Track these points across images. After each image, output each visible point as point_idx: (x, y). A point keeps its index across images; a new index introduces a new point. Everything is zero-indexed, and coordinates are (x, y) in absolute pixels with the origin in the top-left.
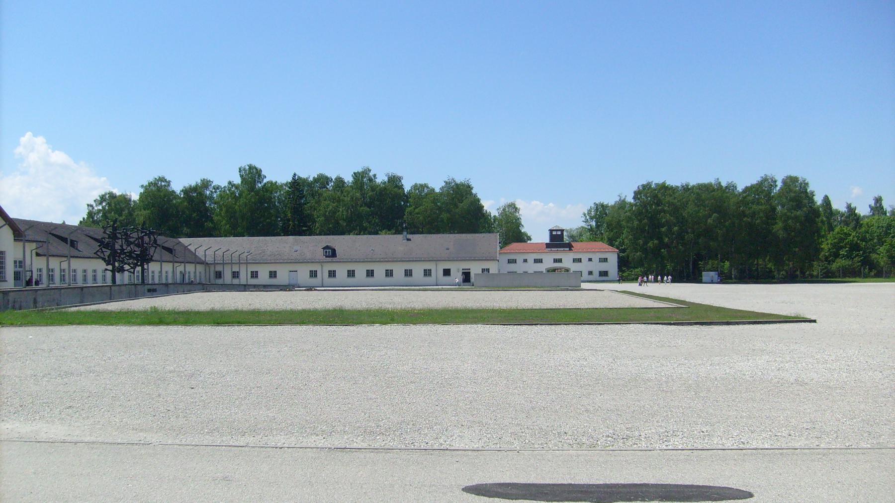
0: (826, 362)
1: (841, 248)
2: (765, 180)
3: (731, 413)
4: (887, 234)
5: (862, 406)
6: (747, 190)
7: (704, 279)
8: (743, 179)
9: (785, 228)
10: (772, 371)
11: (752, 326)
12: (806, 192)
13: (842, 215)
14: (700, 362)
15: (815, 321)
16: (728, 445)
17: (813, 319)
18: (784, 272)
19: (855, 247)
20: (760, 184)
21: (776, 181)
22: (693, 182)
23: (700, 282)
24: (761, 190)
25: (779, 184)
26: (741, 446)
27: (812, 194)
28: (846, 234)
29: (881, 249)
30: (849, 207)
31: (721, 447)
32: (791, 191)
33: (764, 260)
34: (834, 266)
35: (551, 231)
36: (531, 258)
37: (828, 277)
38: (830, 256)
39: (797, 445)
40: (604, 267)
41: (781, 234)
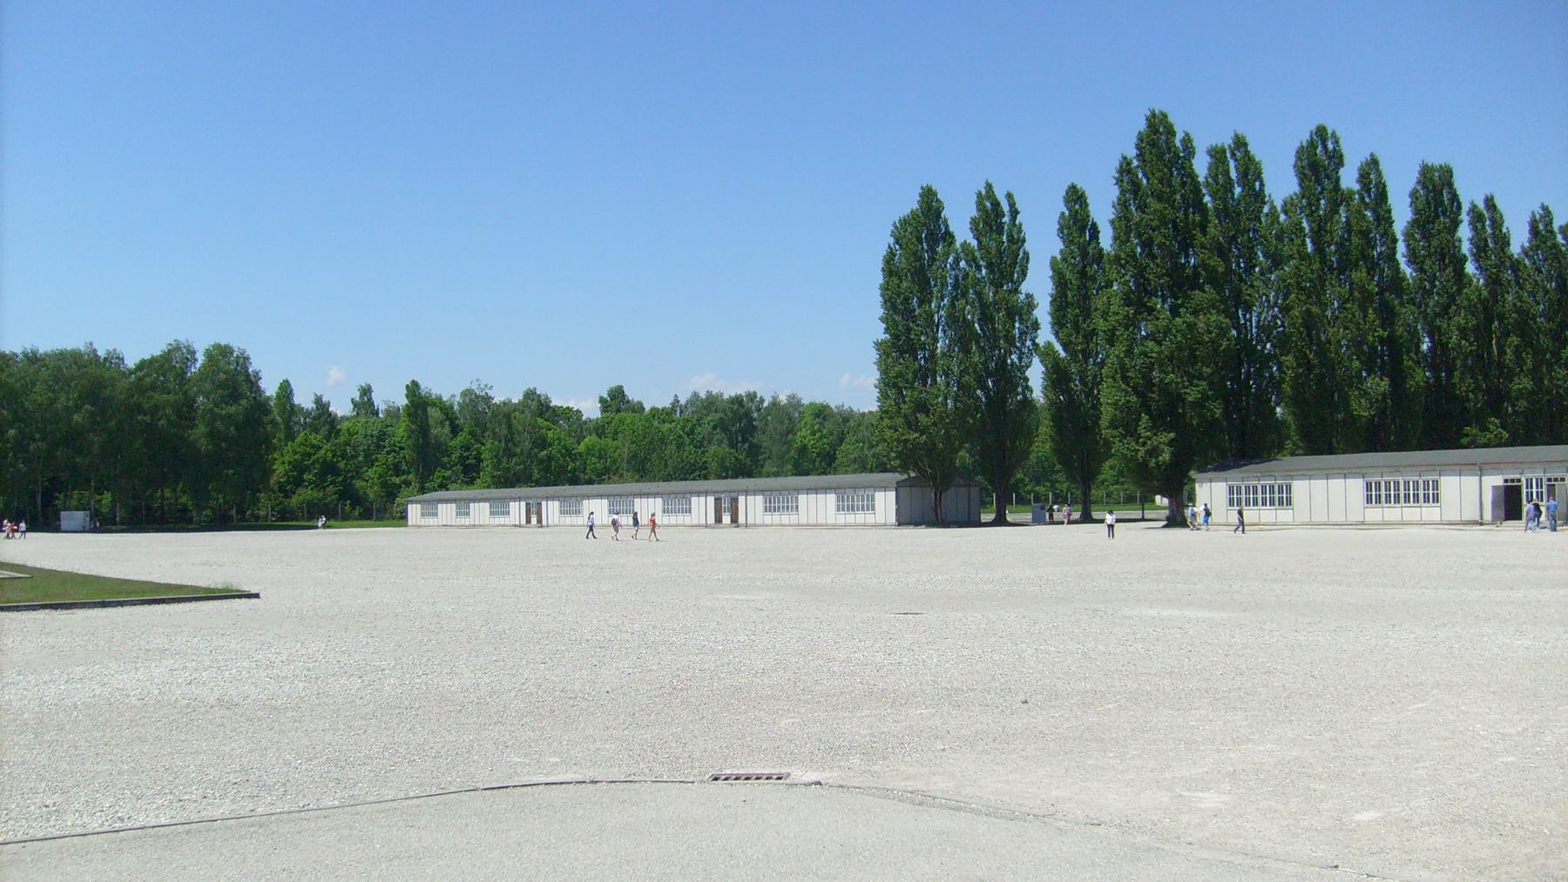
0: (271, 665)
1: (307, 469)
2: (175, 349)
3: (100, 768)
4: (379, 447)
5: (328, 737)
6: (142, 365)
7: (64, 524)
8: (133, 342)
9: (213, 435)
10: (179, 686)
11: (147, 608)
12: (248, 375)
13: (307, 414)
14: (47, 677)
15: (256, 596)
16: (94, 825)
17: (246, 588)
18: (208, 512)
19: (329, 468)
20: (167, 356)
21: (194, 353)
22: (46, 345)
23: (57, 530)
24: (167, 367)
25: (201, 358)
26: (118, 825)
27: (257, 377)
28: (313, 446)
29: (371, 473)
30: (318, 400)
31: (79, 830)
32: (219, 370)
33: (174, 490)
34: (295, 501)
37: (286, 519)
38: (288, 482)
39: (217, 814)
41: (204, 445)
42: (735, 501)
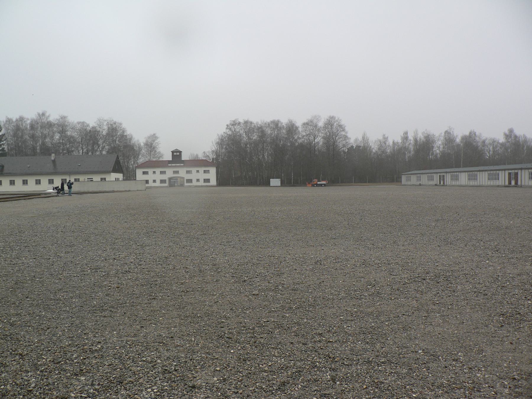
35: (173, 152)
36: (158, 170)
40: (207, 176)
42: (516, 174)
